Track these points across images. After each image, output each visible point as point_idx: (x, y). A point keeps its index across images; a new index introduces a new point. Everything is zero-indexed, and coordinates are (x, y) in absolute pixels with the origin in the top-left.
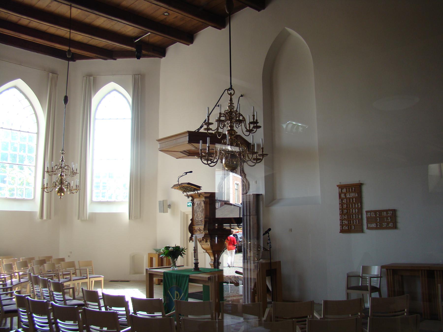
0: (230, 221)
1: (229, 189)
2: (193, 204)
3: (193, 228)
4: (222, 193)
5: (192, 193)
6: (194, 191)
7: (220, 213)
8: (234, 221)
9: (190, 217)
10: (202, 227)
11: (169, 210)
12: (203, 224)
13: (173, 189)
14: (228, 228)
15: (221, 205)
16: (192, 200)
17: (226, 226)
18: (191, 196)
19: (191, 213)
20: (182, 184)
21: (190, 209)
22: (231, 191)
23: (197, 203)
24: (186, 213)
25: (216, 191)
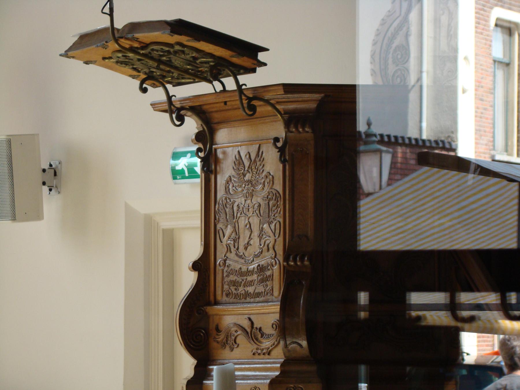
0: (450, 270)
1: (448, 60)
2: (210, 163)
3: (206, 317)
4: (405, 89)
5: (202, 88)
6: (214, 74)
7: (389, 220)
8: (485, 307)
9: (192, 248)
10: (268, 313)
11: (51, 204)
12: (277, 288)
13: (77, 64)
14: (441, 318)
15: (398, 172)
16: (205, 139)
17: (427, 304)
18: (198, 109)
19: (197, 222)
20: (134, 27)
21: (191, 194)
22: (466, 76)
23: (232, 153)
24: (166, 224)
25: (363, 77)
